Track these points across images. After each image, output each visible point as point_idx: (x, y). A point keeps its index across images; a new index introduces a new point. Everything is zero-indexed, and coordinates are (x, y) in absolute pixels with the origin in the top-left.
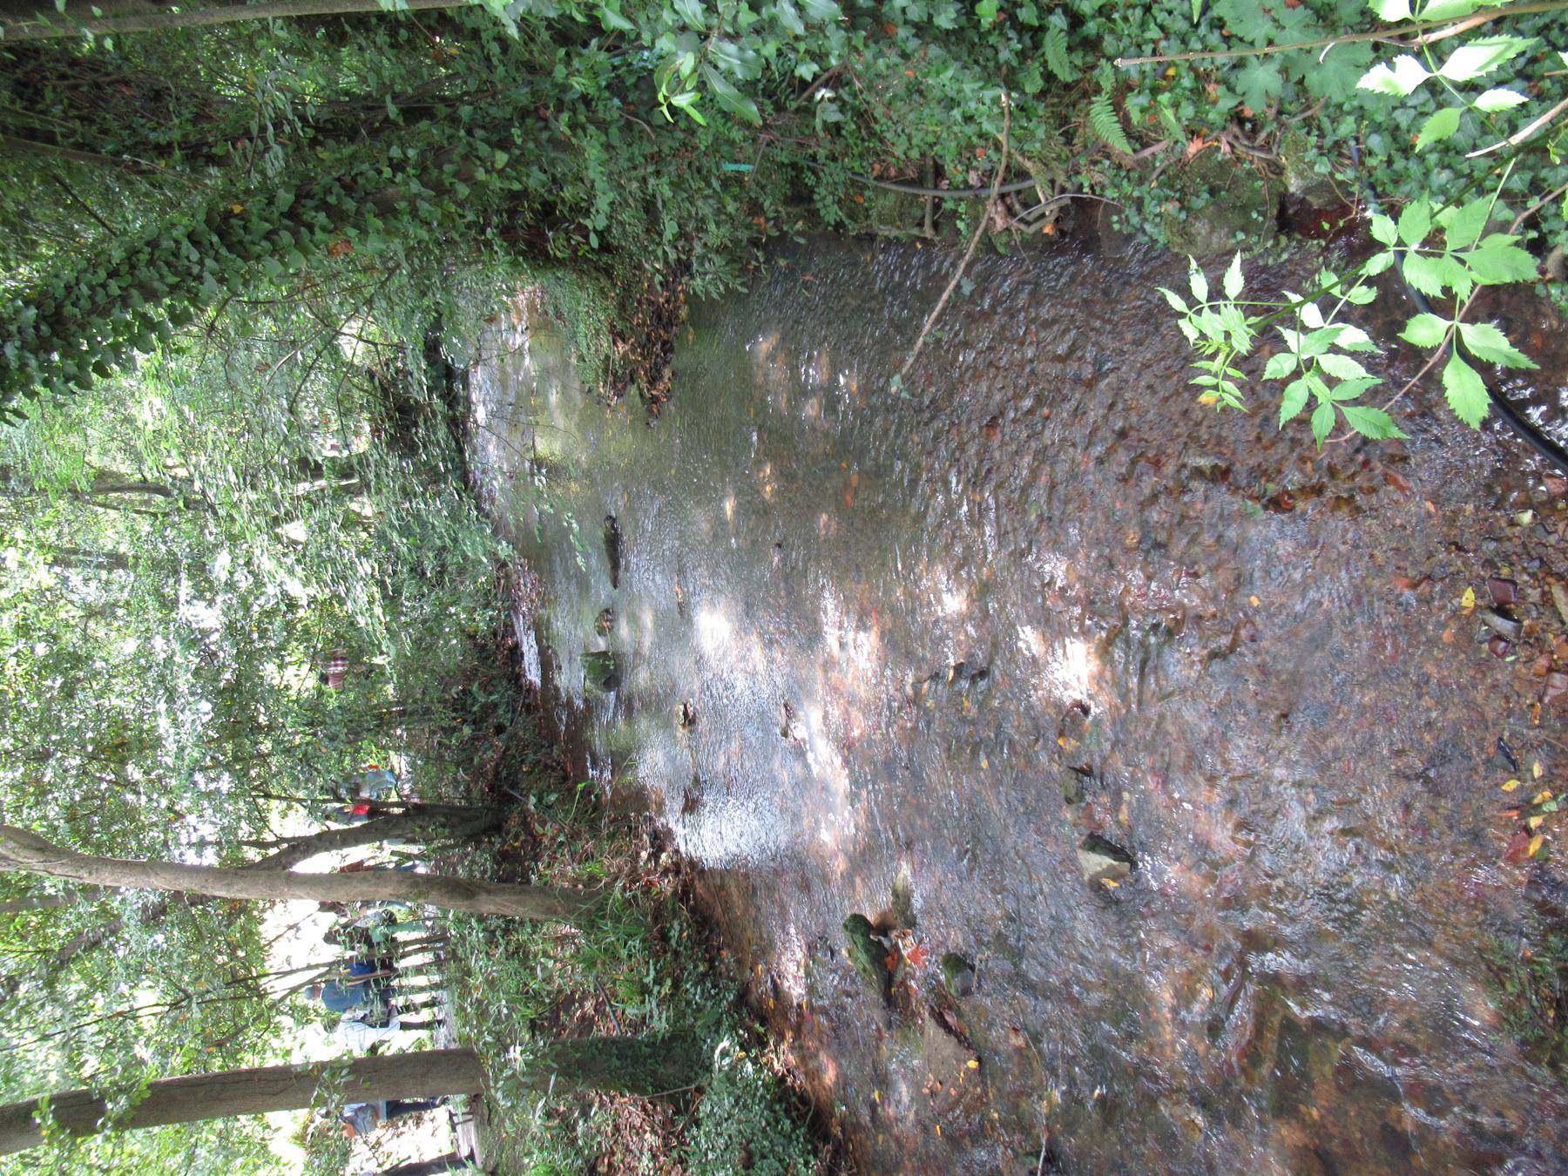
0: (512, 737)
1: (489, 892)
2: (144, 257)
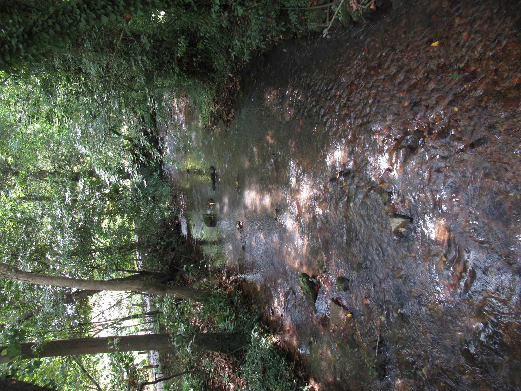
0: (178, 251)
1: (170, 289)
2: (61, 13)
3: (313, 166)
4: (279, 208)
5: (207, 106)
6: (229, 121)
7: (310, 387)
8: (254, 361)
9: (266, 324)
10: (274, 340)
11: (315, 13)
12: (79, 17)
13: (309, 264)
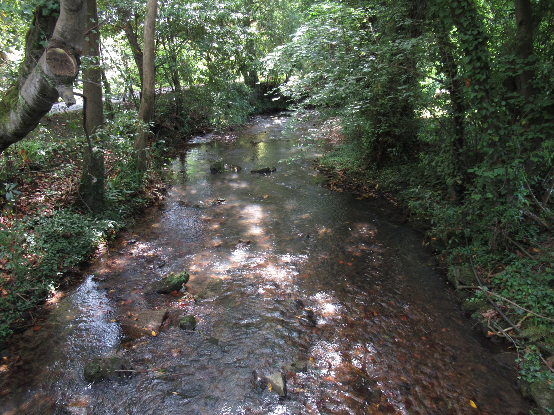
3: (309, 280)
4: (252, 244)
5: (342, 162)
6: (329, 186)
7: (53, 292)
8: (75, 224)
9: (117, 235)
10: (101, 247)
11: (469, 273)
12: (469, 33)
13: (199, 282)
